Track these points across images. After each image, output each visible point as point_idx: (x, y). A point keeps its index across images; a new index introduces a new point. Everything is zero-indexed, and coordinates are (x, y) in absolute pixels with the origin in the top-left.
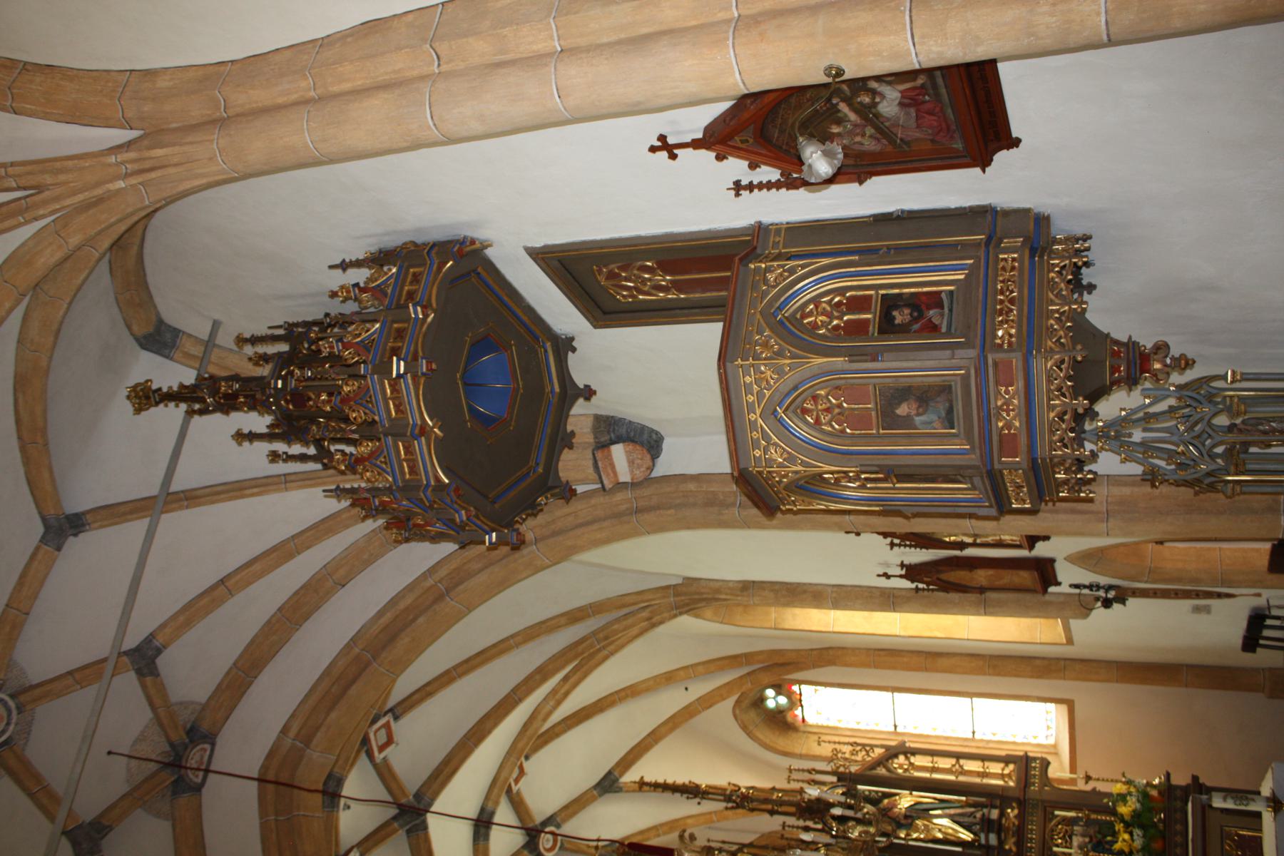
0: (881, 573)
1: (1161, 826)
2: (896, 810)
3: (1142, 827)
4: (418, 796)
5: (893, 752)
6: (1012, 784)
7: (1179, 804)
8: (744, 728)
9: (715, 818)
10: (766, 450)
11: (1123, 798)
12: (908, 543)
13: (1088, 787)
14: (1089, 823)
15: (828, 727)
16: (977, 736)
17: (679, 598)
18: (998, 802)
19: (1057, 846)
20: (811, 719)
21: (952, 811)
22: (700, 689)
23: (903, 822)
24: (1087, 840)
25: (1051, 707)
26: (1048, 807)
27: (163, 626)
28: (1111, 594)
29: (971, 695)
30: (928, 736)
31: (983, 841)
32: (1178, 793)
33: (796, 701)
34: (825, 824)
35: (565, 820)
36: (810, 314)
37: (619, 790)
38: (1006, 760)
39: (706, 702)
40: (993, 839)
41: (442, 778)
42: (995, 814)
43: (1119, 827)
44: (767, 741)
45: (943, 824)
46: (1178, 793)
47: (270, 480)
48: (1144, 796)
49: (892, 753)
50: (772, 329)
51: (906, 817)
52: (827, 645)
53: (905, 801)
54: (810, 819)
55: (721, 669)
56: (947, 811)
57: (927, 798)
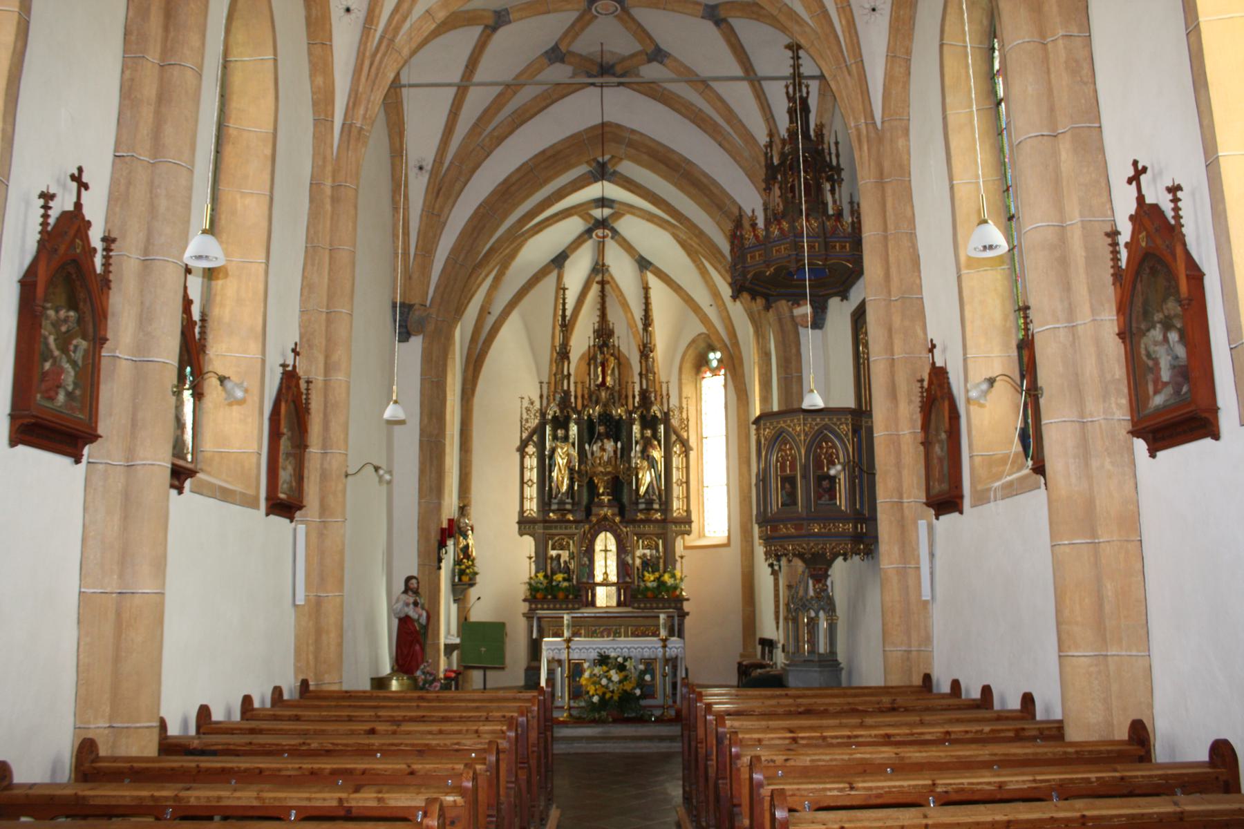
0: (934, 342)
1: (660, 596)
2: (651, 450)
3: (658, 586)
4: (615, 172)
5: (685, 443)
6: (675, 515)
7: (673, 605)
8: (693, 341)
9: (634, 330)
10: (769, 428)
11: (673, 576)
12: (925, 394)
13: (677, 558)
14: (658, 558)
15: (701, 394)
16: (705, 489)
17: (756, 313)
18: (663, 507)
19: (643, 542)
20: (704, 382)
21: (655, 482)
22: (712, 314)
23: (645, 454)
24: (649, 558)
25: (726, 534)
26: (663, 536)
27: (676, 60)
28: (776, 568)
29: (728, 485)
30: (702, 459)
31: (640, 501)
32: (679, 605)
33: (715, 372)
34: (638, 408)
35: (617, 241)
36: (827, 444)
37: (641, 271)
38: (688, 511)
39: (704, 319)
40: (642, 506)
41: (628, 185)
42: (656, 506)
43: (657, 575)
44: (687, 357)
45: (647, 478)
46: (679, 605)
47: (767, 109)
48: (675, 588)
49: (685, 444)
50: (818, 430)
51: (648, 456)
52: (749, 393)
53: (657, 454)
54: (640, 399)
55: (726, 327)
56: (654, 479)
57: (661, 466)
